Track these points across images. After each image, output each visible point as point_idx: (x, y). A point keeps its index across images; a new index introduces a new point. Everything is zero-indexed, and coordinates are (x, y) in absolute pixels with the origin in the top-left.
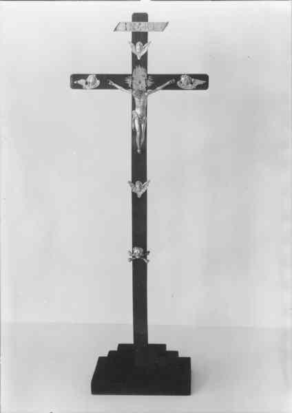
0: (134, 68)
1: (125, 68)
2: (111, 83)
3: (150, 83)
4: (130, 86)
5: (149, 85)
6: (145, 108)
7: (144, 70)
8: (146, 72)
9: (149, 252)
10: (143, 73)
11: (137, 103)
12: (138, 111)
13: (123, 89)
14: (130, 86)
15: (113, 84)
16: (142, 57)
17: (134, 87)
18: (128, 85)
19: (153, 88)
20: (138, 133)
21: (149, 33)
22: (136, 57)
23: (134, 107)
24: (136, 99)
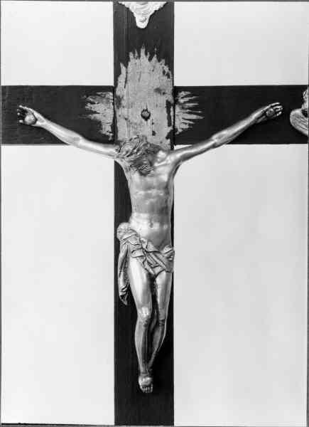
0: (121, 58)
1: (94, 66)
2: (33, 117)
3: (183, 120)
4: (107, 129)
5: (181, 125)
6: (165, 213)
7: (161, 66)
8: (170, 74)
9: (167, 138)
10: (157, 79)
11: (136, 193)
12: (141, 224)
13: (82, 141)
14: (107, 129)
15: (43, 123)
16: (154, 17)
17: (123, 133)
18: (98, 124)
19: (196, 135)
20: (144, 313)
21: (113, 424)
22: (130, 16)
23: (123, 210)
24: (134, 178)
